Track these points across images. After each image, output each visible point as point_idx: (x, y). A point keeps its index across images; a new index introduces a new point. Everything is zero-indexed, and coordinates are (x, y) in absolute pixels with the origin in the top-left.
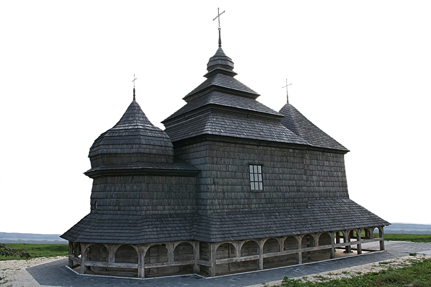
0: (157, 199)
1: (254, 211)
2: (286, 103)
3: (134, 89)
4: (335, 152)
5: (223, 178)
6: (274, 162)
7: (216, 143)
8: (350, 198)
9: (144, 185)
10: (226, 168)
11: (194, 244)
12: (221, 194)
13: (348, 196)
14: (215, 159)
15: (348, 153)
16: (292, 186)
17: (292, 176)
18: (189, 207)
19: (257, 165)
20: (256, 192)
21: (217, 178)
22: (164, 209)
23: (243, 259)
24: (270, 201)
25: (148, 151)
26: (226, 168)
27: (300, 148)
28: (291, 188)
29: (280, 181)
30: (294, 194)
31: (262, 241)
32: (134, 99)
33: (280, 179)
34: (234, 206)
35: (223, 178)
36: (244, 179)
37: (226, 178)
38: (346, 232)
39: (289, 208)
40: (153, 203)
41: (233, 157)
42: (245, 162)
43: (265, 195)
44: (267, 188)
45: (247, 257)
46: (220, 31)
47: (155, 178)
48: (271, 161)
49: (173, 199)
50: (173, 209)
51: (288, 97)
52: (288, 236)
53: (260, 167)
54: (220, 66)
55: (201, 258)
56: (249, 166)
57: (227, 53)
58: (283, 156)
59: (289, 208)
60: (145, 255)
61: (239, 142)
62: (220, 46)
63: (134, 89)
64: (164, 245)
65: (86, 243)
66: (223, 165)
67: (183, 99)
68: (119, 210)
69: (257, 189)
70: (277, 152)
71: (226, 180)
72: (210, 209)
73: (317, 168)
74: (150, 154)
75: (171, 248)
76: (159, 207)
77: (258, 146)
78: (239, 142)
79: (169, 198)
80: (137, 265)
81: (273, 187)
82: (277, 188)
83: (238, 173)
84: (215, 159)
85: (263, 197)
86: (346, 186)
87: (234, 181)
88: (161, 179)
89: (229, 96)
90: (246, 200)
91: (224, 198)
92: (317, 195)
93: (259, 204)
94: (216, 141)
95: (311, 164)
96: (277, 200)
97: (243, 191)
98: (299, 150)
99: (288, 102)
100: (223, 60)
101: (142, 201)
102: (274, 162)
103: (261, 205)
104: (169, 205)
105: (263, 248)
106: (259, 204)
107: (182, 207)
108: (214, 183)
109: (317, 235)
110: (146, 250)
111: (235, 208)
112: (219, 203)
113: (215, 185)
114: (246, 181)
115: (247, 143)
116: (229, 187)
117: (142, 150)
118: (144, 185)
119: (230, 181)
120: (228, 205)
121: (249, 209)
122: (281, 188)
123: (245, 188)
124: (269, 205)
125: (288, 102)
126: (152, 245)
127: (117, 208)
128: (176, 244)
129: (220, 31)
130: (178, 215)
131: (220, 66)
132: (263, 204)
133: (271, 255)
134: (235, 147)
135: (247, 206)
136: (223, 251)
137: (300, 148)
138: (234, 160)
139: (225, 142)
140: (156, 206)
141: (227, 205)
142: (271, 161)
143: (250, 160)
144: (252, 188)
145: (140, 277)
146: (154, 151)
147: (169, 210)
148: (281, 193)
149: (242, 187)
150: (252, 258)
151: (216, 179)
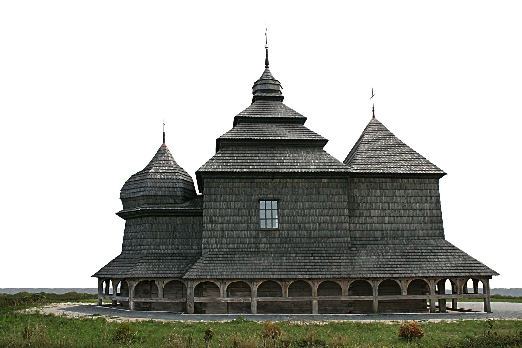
0: (160, 238)
1: (263, 251)
3: (164, 133)
4: (416, 177)
5: (223, 216)
6: (297, 195)
8: (446, 238)
9: (147, 226)
10: (227, 205)
12: (220, 233)
13: (443, 236)
14: (213, 197)
15: (444, 177)
16: (324, 223)
18: (194, 247)
19: (272, 200)
20: (267, 230)
21: (215, 216)
22: (167, 249)
24: (287, 240)
25: (153, 193)
26: (227, 205)
27: (262, 176)
28: (322, 225)
29: (304, 218)
31: (255, 283)
33: (305, 215)
34: (236, 245)
35: (223, 216)
36: (251, 216)
37: (227, 216)
38: (403, 282)
39: (318, 249)
40: (156, 242)
41: (237, 193)
43: (280, 234)
44: (285, 226)
46: (267, 50)
47: (159, 219)
48: (293, 194)
49: (178, 239)
50: (177, 249)
51: (373, 111)
52: (295, 279)
53: (275, 203)
54: (266, 91)
56: (259, 202)
57: (275, 73)
60: (133, 289)
61: (242, 176)
62: (267, 67)
63: (164, 133)
64: (154, 281)
65: (134, 279)
66: (223, 202)
68: (131, 250)
69: (269, 226)
70: (303, 183)
72: (205, 248)
73: (381, 200)
75: (160, 285)
76: (162, 247)
77: (273, 179)
78: (242, 176)
79: (173, 238)
80: (128, 298)
81: (293, 225)
82: (300, 226)
83: (243, 210)
84: (213, 197)
86: (441, 222)
87: (238, 219)
88: (166, 219)
90: (252, 239)
91: (222, 237)
92: (378, 234)
94: (215, 178)
95: (369, 196)
96: (298, 240)
97: (248, 229)
98: (339, 179)
100: (263, 84)
101: (145, 240)
102: (297, 195)
104: (173, 245)
105: (257, 291)
107: (187, 247)
108: (211, 222)
109: (347, 282)
110: (135, 285)
111: (237, 248)
113: (212, 224)
114: (254, 219)
115: (254, 176)
116: (230, 225)
117: (146, 193)
118: (147, 226)
119: (232, 219)
120: (228, 244)
121: (256, 250)
122: (307, 225)
123: (252, 226)
126: (141, 280)
127: (130, 247)
128: (166, 281)
129: (267, 50)
130: (180, 254)
131: (266, 91)
132: (276, 244)
134: (240, 182)
135: (253, 245)
138: (239, 196)
139: (227, 178)
140: (159, 245)
141: (226, 243)
142: (293, 194)
143: (261, 195)
145: (130, 309)
146: (160, 193)
147: (172, 249)
148: (305, 232)
149: (248, 226)
150: (241, 300)
151: (213, 217)
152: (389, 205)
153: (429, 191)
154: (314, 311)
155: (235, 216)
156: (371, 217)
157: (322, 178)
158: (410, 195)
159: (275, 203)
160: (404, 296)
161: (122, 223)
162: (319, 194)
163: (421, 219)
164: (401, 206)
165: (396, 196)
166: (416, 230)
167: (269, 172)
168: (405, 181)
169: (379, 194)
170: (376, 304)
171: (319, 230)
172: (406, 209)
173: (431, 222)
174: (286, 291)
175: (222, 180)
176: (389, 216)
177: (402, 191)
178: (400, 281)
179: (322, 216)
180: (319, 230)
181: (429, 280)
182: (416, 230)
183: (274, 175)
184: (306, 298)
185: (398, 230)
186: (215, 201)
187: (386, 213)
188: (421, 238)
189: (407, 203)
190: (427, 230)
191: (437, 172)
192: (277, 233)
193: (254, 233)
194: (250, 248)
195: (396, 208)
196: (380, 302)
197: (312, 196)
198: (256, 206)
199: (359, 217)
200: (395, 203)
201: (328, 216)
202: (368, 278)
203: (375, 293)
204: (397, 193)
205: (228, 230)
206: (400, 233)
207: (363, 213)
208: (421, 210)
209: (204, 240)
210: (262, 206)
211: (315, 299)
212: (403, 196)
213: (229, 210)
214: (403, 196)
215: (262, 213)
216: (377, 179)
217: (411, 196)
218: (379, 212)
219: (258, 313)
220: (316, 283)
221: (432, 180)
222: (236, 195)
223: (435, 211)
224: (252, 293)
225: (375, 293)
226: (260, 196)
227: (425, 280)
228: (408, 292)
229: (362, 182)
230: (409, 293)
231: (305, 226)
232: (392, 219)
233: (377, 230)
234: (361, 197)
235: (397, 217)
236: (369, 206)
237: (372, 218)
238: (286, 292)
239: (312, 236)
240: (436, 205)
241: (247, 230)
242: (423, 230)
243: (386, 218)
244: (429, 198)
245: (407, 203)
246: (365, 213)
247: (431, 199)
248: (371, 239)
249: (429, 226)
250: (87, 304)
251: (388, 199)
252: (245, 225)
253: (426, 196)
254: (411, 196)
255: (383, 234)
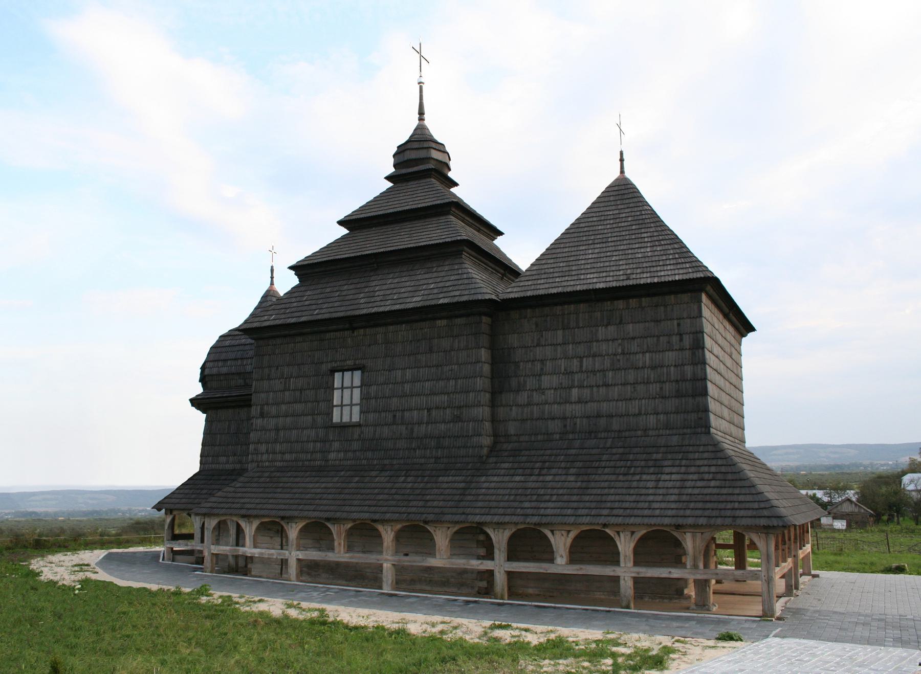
0: (220, 445)
2: (617, 174)
3: (621, 153)
7: (328, 336)
11: (334, 529)
12: (273, 434)
14: (266, 371)
16: (437, 408)
17: (441, 383)
22: (227, 462)
23: (460, 563)
27: (335, 327)
28: (434, 412)
30: (443, 427)
32: (272, 284)
33: (404, 395)
38: (557, 533)
39: (423, 461)
42: (325, 368)
43: (362, 432)
44: (371, 417)
45: (263, 551)
46: (421, 88)
51: (622, 160)
55: (491, 573)
57: (438, 135)
58: (418, 341)
59: (423, 461)
62: (421, 119)
63: (621, 153)
67: (340, 223)
69: (346, 419)
71: (284, 407)
72: (252, 461)
74: (219, 375)
77: (354, 329)
80: (385, 565)
82: (395, 416)
84: (266, 371)
85: (356, 437)
89: (408, 225)
91: (276, 441)
92: (554, 426)
93: (346, 451)
95: (538, 345)
99: (622, 172)
103: (350, 455)
104: (235, 455)
106: (346, 451)
108: (262, 415)
111: (296, 460)
112: (267, 450)
122: (407, 414)
124: (369, 454)
125: (622, 172)
129: (421, 88)
132: (355, 451)
133: (314, 555)
136: (271, 537)
137: (335, 327)
144: (336, 418)
146: (224, 370)
148: (404, 427)
149: (313, 420)
150: (272, 554)
152: (581, 362)
153: (675, 322)
154: (385, 585)
155: (296, 402)
156: (541, 390)
157: (435, 319)
158: (631, 335)
159: (357, 374)
160: (561, 564)
161: (200, 418)
162: (431, 351)
163: (654, 388)
164: (607, 363)
165: (597, 341)
166: (640, 414)
167: (697, 278)
168: (620, 304)
169: (560, 340)
170: (500, 580)
171: (427, 423)
172: (619, 369)
173: (679, 395)
174: (340, 542)
175: (279, 341)
176: (581, 387)
177: (611, 329)
178: (552, 532)
179: (435, 394)
180: (427, 423)
181: (618, 533)
182: (640, 414)
183: (352, 323)
184: (371, 558)
185: (599, 416)
186: (269, 379)
187: (573, 381)
188: (651, 433)
189: (623, 353)
190: (666, 413)
191: (695, 276)
192: (357, 431)
193: (321, 433)
194: (315, 460)
195: (597, 367)
196: (636, 581)
197: (419, 357)
198: (327, 383)
199: (518, 391)
200: (594, 356)
201: (445, 394)
202: (540, 524)
203: (500, 554)
204: (602, 332)
205: (284, 429)
206: (603, 422)
207: (525, 382)
208: (653, 368)
209: (252, 447)
210: (337, 384)
211: (387, 560)
212: (613, 340)
213: (287, 393)
214: (613, 340)
215: (337, 394)
216: (559, 308)
217: (633, 338)
218: (559, 379)
219: (298, 580)
220: (389, 529)
221: (685, 297)
222: (299, 365)
223: (689, 370)
224: (290, 543)
225: (500, 554)
226: (334, 365)
227: (607, 531)
228: (634, 562)
229: (526, 317)
230: (572, 561)
231: (403, 417)
232: (586, 392)
233: (553, 419)
234: (524, 350)
235: (598, 386)
236: (538, 366)
237: (543, 393)
238: (340, 544)
239: (415, 435)
240: (694, 354)
241: (312, 428)
242: (657, 414)
243: (575, 391)
244: (675, 339)
245: (623, 353)
246: (531, 383)
247: (681, 340)
248: (540, 437)
249: (671, 404)
250: (131, 550)
251: (581, 350)
252: (310, 418)
253: (670, 335)
254: (633, 338)
255: (565, 426)
